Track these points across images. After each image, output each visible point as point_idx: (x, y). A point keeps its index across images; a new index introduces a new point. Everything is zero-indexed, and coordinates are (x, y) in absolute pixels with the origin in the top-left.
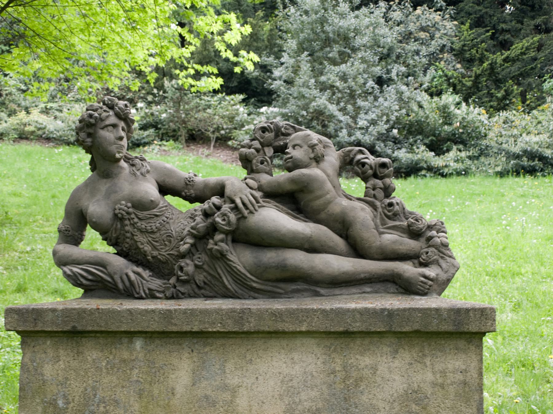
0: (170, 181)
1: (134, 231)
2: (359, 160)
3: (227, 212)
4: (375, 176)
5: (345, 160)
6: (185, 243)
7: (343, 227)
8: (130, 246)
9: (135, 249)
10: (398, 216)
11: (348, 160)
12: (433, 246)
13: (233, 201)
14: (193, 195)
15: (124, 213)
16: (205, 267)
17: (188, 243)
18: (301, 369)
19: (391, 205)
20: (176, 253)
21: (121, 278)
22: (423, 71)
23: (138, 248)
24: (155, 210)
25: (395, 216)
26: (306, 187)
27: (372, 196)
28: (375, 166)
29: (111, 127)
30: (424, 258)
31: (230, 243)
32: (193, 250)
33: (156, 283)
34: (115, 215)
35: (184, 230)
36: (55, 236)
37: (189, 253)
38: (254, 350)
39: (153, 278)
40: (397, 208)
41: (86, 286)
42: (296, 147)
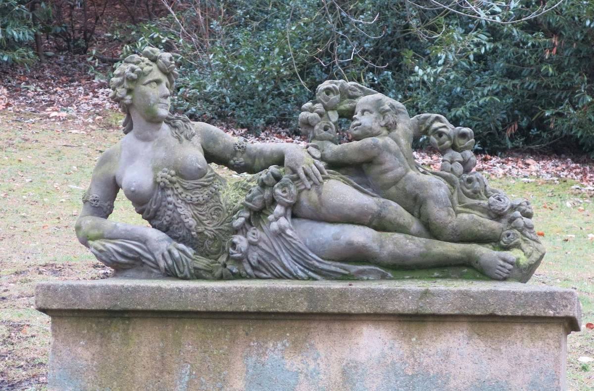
0: (216, 149)
1: (178, 203)
2: (436, 129)
3: (288, 183)
4: (454, 147)
5: (420, 128)
6: (238, 217)
7: (415, 203)
8: (172, 219)
9: (178, 224)
10: (478, 194)
11: (423, 129)
12: (515, 228)
13: (294, 171)
14: (243, 163)
15: (167, 181)
16: (262, 245)
17: (242, 217)
18: (366, 355)
19: (470, 181)
20: (226, 228)
21: (163, 255)
22: (496, 52)
23: (182, 221)
24: (202, 179)
25: (475, 194)
26: (374, 157)
27: (450, 170)
28: (454, 136)
29: (155, 83)
30: (505, 241)
31: (289, 218)
32: (247, 226)
33: (202, 262)
34: (156, 183)
35: (236, 202)
36: (79, 208)
37: (242, 228)
38: (316, 333)
39: (198, 256)
40: (477, 185)
41: (118, 263)
42: (365, 113)
